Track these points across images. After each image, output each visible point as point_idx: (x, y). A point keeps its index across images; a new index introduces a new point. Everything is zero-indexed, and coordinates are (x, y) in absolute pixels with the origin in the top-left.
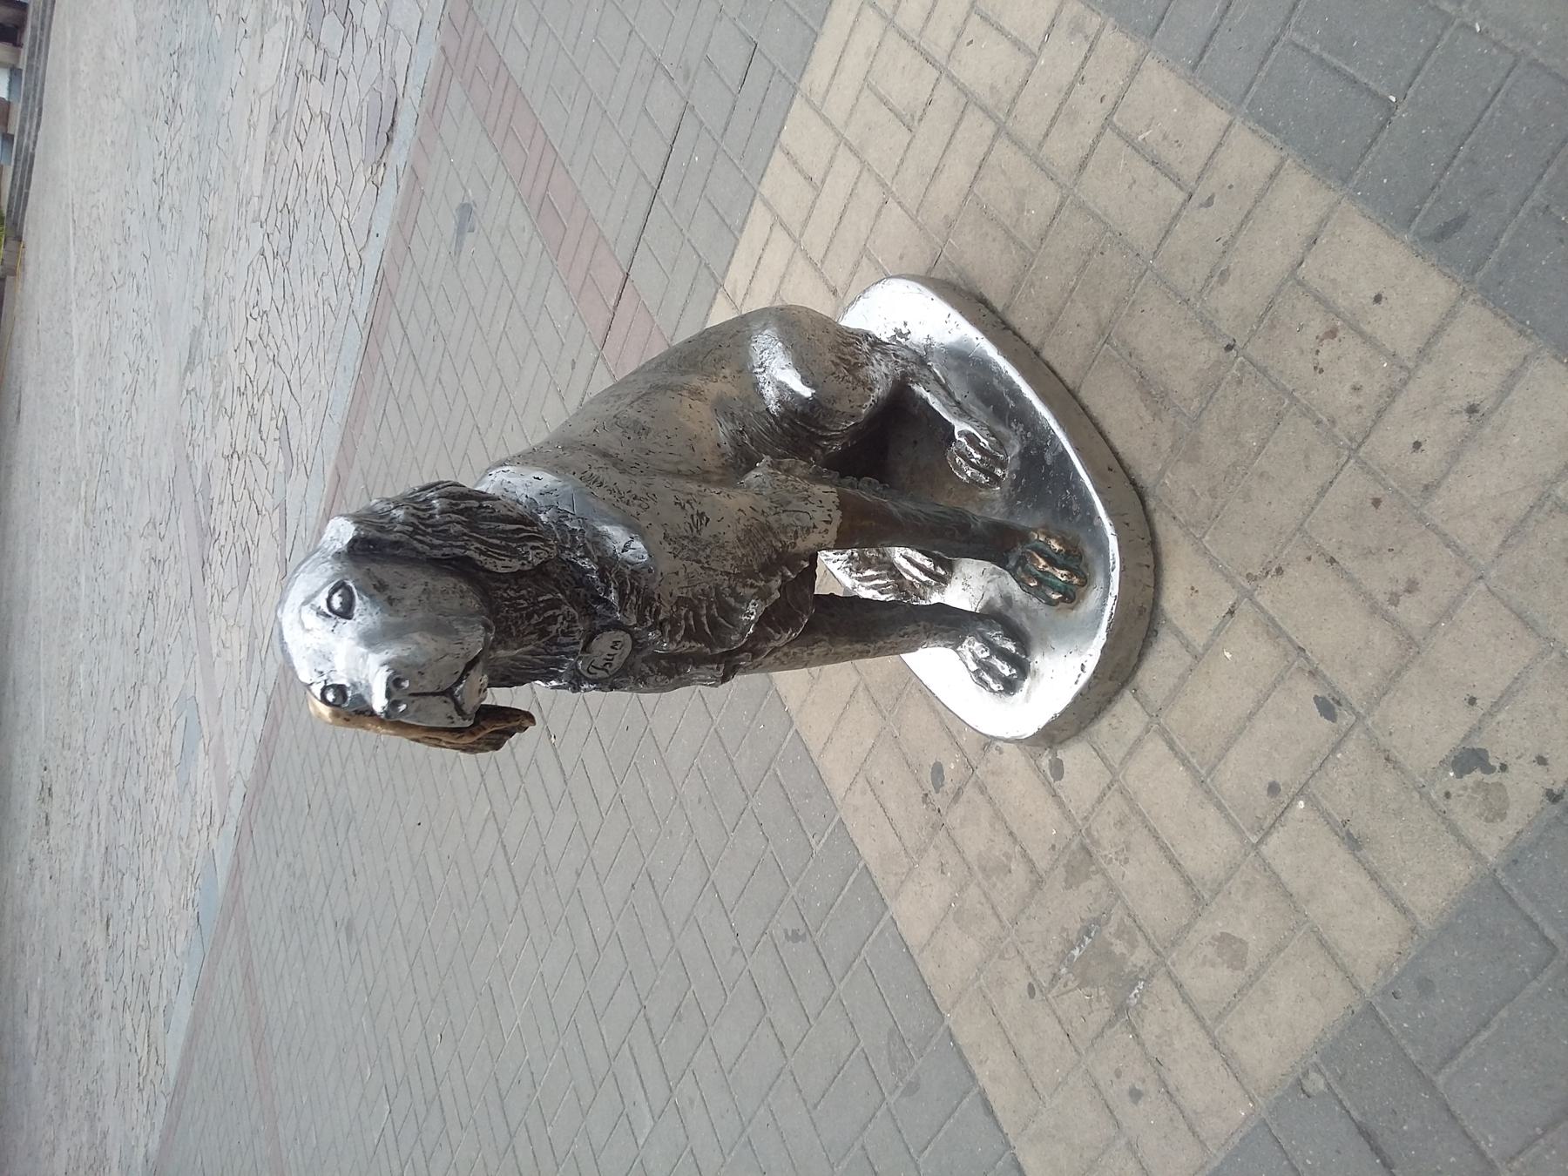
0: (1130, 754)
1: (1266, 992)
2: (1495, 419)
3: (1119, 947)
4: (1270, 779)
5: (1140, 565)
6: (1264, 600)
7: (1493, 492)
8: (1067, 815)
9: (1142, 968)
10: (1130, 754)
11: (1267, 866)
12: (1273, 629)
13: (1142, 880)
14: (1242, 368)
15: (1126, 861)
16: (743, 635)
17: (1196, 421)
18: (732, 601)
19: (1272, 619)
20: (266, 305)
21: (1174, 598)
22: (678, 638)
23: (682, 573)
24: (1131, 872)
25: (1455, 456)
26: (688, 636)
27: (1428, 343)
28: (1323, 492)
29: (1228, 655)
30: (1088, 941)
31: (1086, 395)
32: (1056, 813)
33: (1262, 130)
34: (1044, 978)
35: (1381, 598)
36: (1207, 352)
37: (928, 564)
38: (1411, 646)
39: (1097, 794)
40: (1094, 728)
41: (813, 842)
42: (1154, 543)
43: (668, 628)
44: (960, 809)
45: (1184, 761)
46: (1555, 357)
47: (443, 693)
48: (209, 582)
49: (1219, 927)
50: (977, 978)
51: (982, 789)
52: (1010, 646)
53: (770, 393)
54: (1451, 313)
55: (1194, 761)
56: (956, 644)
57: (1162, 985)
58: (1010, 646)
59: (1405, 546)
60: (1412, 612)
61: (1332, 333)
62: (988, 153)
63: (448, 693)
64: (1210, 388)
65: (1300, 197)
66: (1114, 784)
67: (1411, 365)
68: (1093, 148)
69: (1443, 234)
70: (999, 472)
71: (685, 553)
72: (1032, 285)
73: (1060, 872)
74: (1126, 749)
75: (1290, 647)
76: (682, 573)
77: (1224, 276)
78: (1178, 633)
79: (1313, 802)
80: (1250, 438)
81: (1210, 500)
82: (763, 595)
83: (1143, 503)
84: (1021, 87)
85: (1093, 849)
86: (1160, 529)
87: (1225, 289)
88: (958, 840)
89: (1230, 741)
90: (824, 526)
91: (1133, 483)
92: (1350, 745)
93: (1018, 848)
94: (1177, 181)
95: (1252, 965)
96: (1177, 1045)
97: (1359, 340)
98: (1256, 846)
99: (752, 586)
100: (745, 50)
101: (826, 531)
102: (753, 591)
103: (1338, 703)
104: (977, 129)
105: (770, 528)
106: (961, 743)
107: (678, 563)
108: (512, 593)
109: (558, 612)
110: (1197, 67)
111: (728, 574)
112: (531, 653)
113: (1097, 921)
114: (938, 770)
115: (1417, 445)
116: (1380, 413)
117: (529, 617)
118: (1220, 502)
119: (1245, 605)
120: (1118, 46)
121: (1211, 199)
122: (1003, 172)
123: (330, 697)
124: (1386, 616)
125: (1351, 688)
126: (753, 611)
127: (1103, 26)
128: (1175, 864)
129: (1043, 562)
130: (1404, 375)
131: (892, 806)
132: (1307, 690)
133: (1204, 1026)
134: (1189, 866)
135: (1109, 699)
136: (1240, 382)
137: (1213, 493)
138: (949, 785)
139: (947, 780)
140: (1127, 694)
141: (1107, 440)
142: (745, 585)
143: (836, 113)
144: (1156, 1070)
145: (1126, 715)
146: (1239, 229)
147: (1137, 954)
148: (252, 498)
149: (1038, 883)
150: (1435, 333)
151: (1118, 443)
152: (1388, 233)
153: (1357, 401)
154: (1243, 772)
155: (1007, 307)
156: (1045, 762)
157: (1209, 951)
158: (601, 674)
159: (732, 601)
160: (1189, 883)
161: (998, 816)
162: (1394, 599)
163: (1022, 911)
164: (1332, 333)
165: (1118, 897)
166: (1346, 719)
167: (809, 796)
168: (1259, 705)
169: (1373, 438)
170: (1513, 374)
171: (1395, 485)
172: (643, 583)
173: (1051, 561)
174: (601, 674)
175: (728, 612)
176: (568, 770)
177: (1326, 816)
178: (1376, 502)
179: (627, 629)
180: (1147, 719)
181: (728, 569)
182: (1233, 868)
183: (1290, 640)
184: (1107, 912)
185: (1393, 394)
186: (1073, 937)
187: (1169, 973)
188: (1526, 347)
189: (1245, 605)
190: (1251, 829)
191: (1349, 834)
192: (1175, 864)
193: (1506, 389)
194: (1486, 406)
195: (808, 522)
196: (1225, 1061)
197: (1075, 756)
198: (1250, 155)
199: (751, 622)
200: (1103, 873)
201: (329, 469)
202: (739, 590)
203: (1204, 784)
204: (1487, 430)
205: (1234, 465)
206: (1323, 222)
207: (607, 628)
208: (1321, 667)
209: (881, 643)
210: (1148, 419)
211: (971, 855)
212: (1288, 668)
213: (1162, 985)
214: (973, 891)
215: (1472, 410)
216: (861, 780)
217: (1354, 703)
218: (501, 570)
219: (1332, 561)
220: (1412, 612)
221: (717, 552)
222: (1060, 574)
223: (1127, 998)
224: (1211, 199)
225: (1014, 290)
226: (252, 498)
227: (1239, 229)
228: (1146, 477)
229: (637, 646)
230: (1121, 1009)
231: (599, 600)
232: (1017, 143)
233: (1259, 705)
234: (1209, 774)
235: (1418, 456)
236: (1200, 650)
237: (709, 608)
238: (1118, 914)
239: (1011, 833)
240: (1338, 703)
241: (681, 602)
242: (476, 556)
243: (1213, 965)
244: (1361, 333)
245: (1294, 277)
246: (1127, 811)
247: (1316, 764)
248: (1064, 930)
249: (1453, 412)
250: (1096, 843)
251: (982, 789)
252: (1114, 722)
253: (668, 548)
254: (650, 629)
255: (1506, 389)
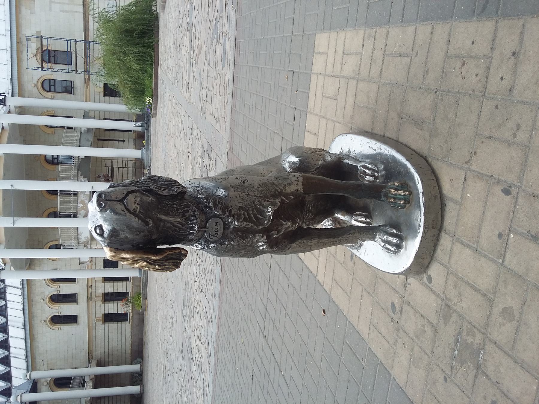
0: (450, 256)
1: (525, 324)
2: (522, 51)
3: (470, 340)
4: (498, 232)
5: (430, 179)
6: (474, 167)
7: (531, 75)
8: (438, 296)
9: (480, 343)
10: (450, 256)
11: (509, 269)
12: (480, 175)
13: (470, 306)
14: (442, 95)
15: (461, 300)
16: (269, 220)
17: (434, 122)
18: (261, 207)
19: (479, 173)
20: (199, 275)
21: (447, 188)
22: (241, 220)
23: (238, 197)
24: (464, 305)
25: (515, 72)
26: (245, 220)
27: (493, 44)
28: (479, 116)
29: (469, 195)
30: (458, 344)
31: (400, 140)
32: (434, 297)
33: (425, 23)
34: (448, 372)
35: (510, 138)
36: (430, 97)
37: (363, 219)
38: (526, 148)
39: (444, 280)
40: (436, 255)
41: (363, 363)
42: (433, 172)
43: (236, 217)
44: (404, 317)
45: (468, 246)
46: (532, 17)
47: (119, 201)
48: (193, 378)
49: (501, 307)
50: (427, 385)
51: (409, 304)
52: (394, 231)
53: (287, 166)
54: (496, 30)
55: (471, 244)
56: (373, 238)
57: (489, 347)
58: (394, 231)
59: (511, 114)
60: (522, 136)
61: (464, 64)
62: (357, 89)
63: (121, 201)
64: (434, 109)
65: (441, 30)
66: (450, 272)
67: (490, 55)
68: (382, 65)
69: (484, 9)
70: (376, 174)
71: (239, 190)
72: (377, 117)
73: (442, 321)
74: (448, 256)
75: (487, 178)
76: (238, 197)
77: (427, 72)
78: (452, 200)
79: (515, 232)
80: (452, 116)
81: (446, 145)
82: (273, 204)
83: (427, 161)
84: (360, 64)
85: (449, 304)
86: (435, 166)
87: (429, 74)
88: (406, 330)
89: (480, 227)
90: (297, 182)
91: (422, 157)
92: (520, 200)
93: (426, 320)
94: (407, 56)
95: (517, 316)
96: (502, 370)
97: (472, 60)
98: (502, 264)
99: (268, 201)
100: (293, 111)
101: (297, 184)
102: (269, 203)
103: (510, 187)
104: (353, 84)
105: (274, 184)
106: (397, 289)
107: (236, 193)
108: (170, 203)
109: (189, 209)
110: (403, 21)
111: (257, 196)
112: (179, 223)
113: (459, 334)
114: (393, 305)
115: (502, 78)
116: (487, 78)
117: (178, 210)
118: (450, 143)
119: (469, 173)
120: (381, 32)
121: (417, 53)
122: (362, 91)
123: (98, 231)
124: (514, 144)
125: (511, 178)
126: (270, 211)
127: (376, 31)
128: (477, 290)
129: (392, 191)
130: (489, 60)
131: (383, 331)
132: (498, 190)
133: (509, 356)
134: (482, 288)
135: (437, 238)
136: (442, 100)
137: (446, 142)
138: (398, 309)
139: (397, 308)
140: (443, 234)
141: (411, 149)
142: (265, 201)
143: (317, 111)
144: (498, 388)
145: (445, 241)
146: (428, 55)
147: (476, 338)
148: (200, 341)
149: (436, 330)
150: (494, 40)
151: (414, 147)
152: (469, 22)
153: (478, 78)
154: (488, 237)
155: (372, 129)
156: (425, 279)
157: (500, 320)
158: (215, 238)
159: (261, 207)
160: (485, 295)
161: (416, 311)
162: (514, 136)
163: (434, 346)
164: (464, 64)
165: (463, 318)
166: (514, 191)
167: (358, 345)
168: (485, 207)
169: (488, 87)
170: (521, 33)
171: (500, 97)
172: (224, 202)
173: (396, 189)
174: (215, 238)
175: (262, 213)
176: (288, 383)
177: (522, 234)
178: (497, 107)
179: (218, 217)
180: (452, 239)
181: (256, 194)
182: (498, 277)
183: (487, 176)
184: (461, 327)
185: (488, 68)
186: (453, 346)
187: (490, 340)
188: (521, 22)
189: (469, 173)
190: (498, 257)
191: (532, 236)
192: (477, 290)
193: (521, 40)
194: (517, 50)
195: (289, 181)
196: (521, 366)
197: (435, 270)
198: (424, 30)
199: (270, 215)
200: (455, 311)
201: (217, 317)
202: (263, 202)
203: (477, 251)
204: (521, 57)
205: (449, 128)
206: (449, 34)
207: (211, 218)
208: (500, 178)
209: (340, 238)
210: (420, 132)
211: (412, 334)
212: (489, 186)
213: (489, 347)
214: (416, 348)
215: (514, 54)
216: (372, 327)
217: (515, 183)
218: (164, 194)
219: (490, 137)
220: (522, 136)
221: (251, 189)
222: (401, 193)
223: (479, 361)
224: (417, 53)
225: (373, 123)
226: (200, 341)
227: (428, 55)
228: (425, 152)
229: (226, 226)
230: (478, 367)
231: (207, 207)
232: (364, 80)
233: (485, 207)
234: (477, 245)
235: (504, 81)
236: (460, 200)
237: (253, 211)
238: (465, 324)
239: (422, 316)
240: (510, 187)
241: (240, 208)
242: (154, 189)
243: (504, 325)
244: (472, 57)
245: (447, 54)
246: (455, 279)
247: (511, 216)
248: (449, 344)
249: (508, 60)
250: (450, 300)
251: (409, 304)
252: (442, 247)
253: (232, 189)
254: (228, 216)
255: (521, 40)
